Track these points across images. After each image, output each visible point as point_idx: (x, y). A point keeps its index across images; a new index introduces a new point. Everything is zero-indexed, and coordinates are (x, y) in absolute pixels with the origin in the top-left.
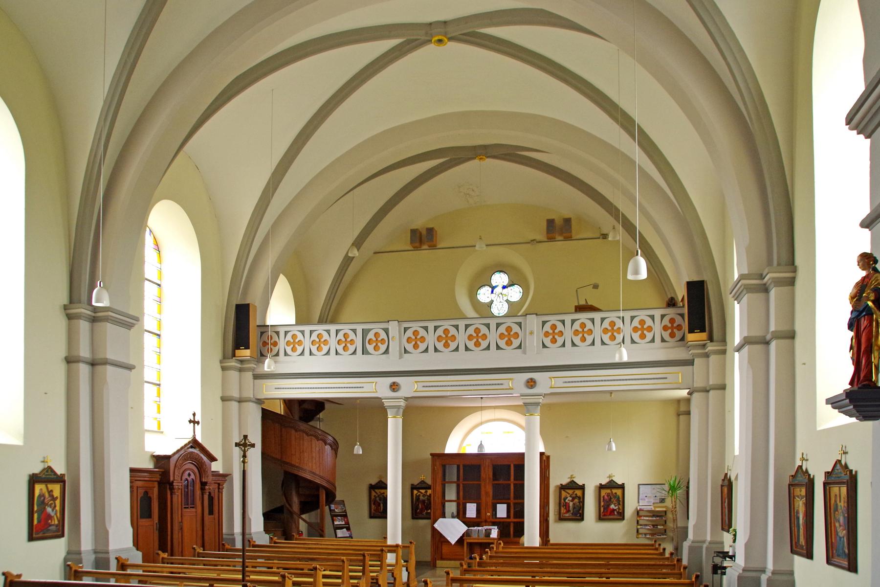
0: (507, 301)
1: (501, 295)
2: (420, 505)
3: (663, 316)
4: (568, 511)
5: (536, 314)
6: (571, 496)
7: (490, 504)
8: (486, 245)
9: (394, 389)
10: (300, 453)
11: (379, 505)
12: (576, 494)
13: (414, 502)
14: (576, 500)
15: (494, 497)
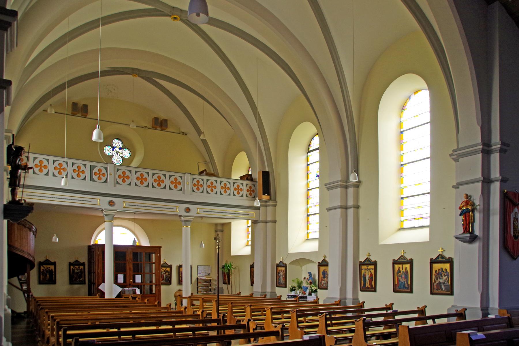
0: (122, 157)
1: (118, 153)
2: (75, 275)
3: (247, 185)
4: (163, 279)
5: (190, 174)
6: (164, 271)
7: (132, 274)
8: (136, 126)
9: (111, 205)
10: (21, 239)
11: (46, 275)
12: (167, 270)
13: (71, 274)
14: (167, 273)
15: (134, 271)
